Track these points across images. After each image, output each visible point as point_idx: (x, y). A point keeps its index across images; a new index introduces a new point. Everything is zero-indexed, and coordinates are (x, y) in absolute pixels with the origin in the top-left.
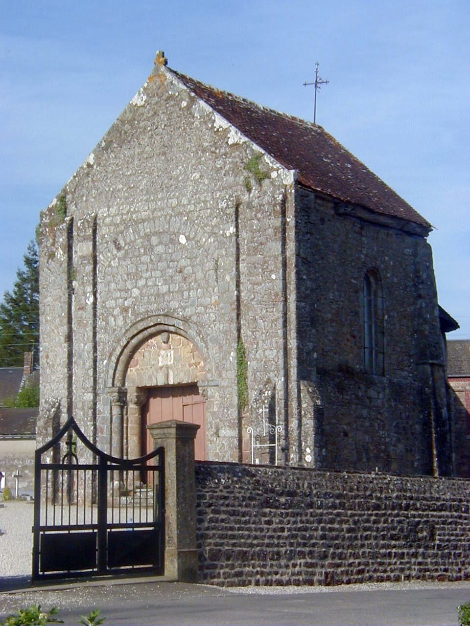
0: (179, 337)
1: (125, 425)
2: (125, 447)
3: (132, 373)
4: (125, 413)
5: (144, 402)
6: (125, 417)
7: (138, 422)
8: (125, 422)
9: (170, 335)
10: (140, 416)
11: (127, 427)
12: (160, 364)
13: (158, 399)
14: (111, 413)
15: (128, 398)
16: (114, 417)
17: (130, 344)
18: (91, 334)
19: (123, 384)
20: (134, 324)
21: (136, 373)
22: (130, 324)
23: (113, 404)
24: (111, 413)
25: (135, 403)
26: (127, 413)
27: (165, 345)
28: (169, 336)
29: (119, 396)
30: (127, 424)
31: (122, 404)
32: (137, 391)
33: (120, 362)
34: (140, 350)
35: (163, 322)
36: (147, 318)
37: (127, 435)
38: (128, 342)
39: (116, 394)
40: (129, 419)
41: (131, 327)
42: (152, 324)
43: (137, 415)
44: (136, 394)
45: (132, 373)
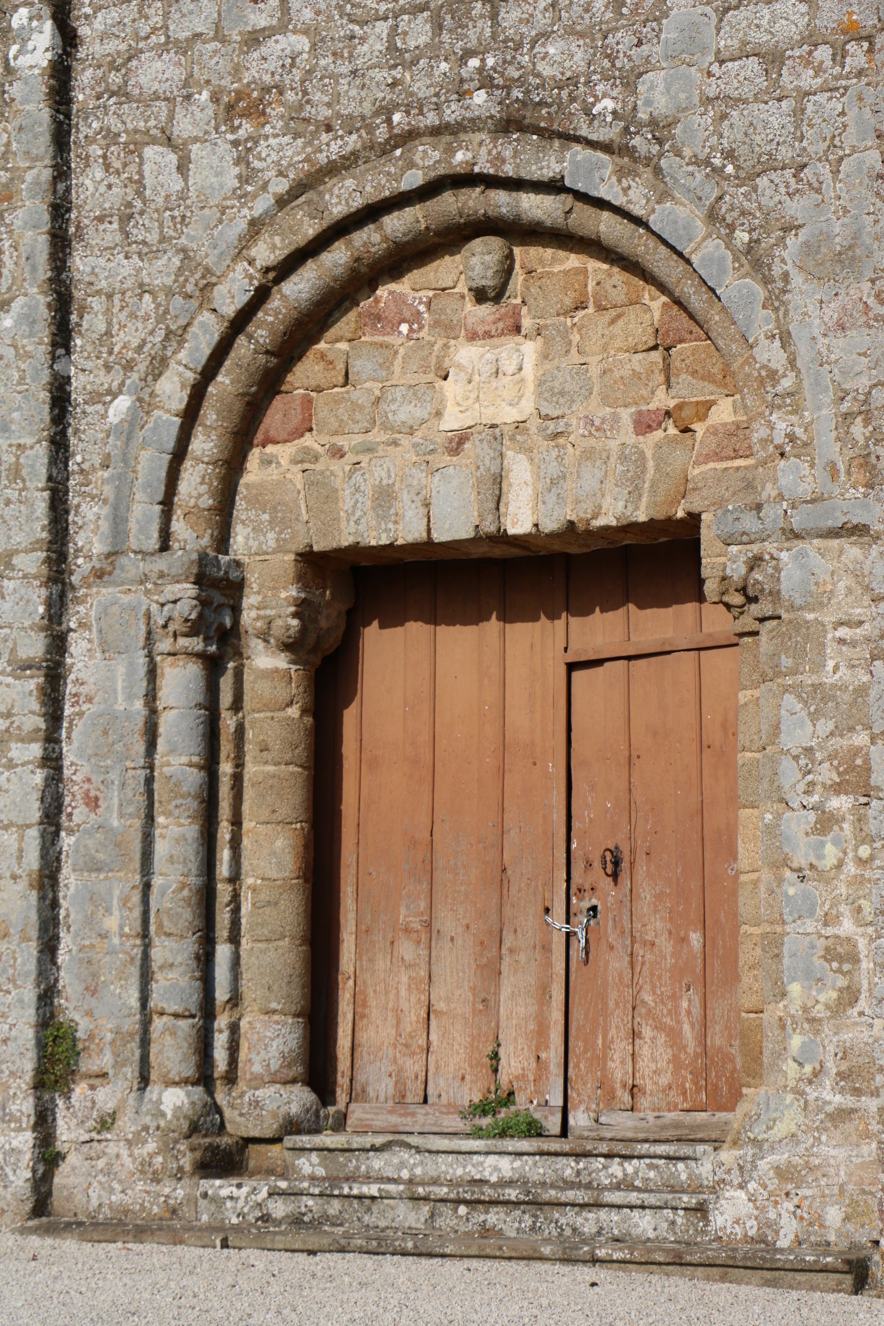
0: (573, 260)
1: (226, 768)
2: (223, 891)
3: (272, 474)
4: (226, 698)
5: (332, 642)
6: (228, 722)
7: (301, 752)
8: (226, 748)
9: (517, 250)
10: (309, 720)
11: (237, 779)
12: (452, 421)
13: (416, 629)
14: (151, 697)
15: (248, 617)
16: (167, 723)
17: (275, 303)
18: (41, 244)
19: (223, 542)
20: (299, 189)
21: (299, 480)
22: (281, 186)
23: (164, 645)
24: (151, 697)
25: (288, 647)
26: (237, 705)
27: (486, 310)
28: (510, 257)
29: (203, 602)
30: (239, 764)
31: (213, 648)
32: (301, 578)
33: (209, 415)
34: (322, 345)
35: (483, 167)
36: (385, 150)
37: (237, 822)
38: (261, 296)
39: (188, 590)
40: (249, 734)
41: (282, 202)
42: (413, 179)
43: (294, 712)
44: (293, 592)
45: (272, 474)
